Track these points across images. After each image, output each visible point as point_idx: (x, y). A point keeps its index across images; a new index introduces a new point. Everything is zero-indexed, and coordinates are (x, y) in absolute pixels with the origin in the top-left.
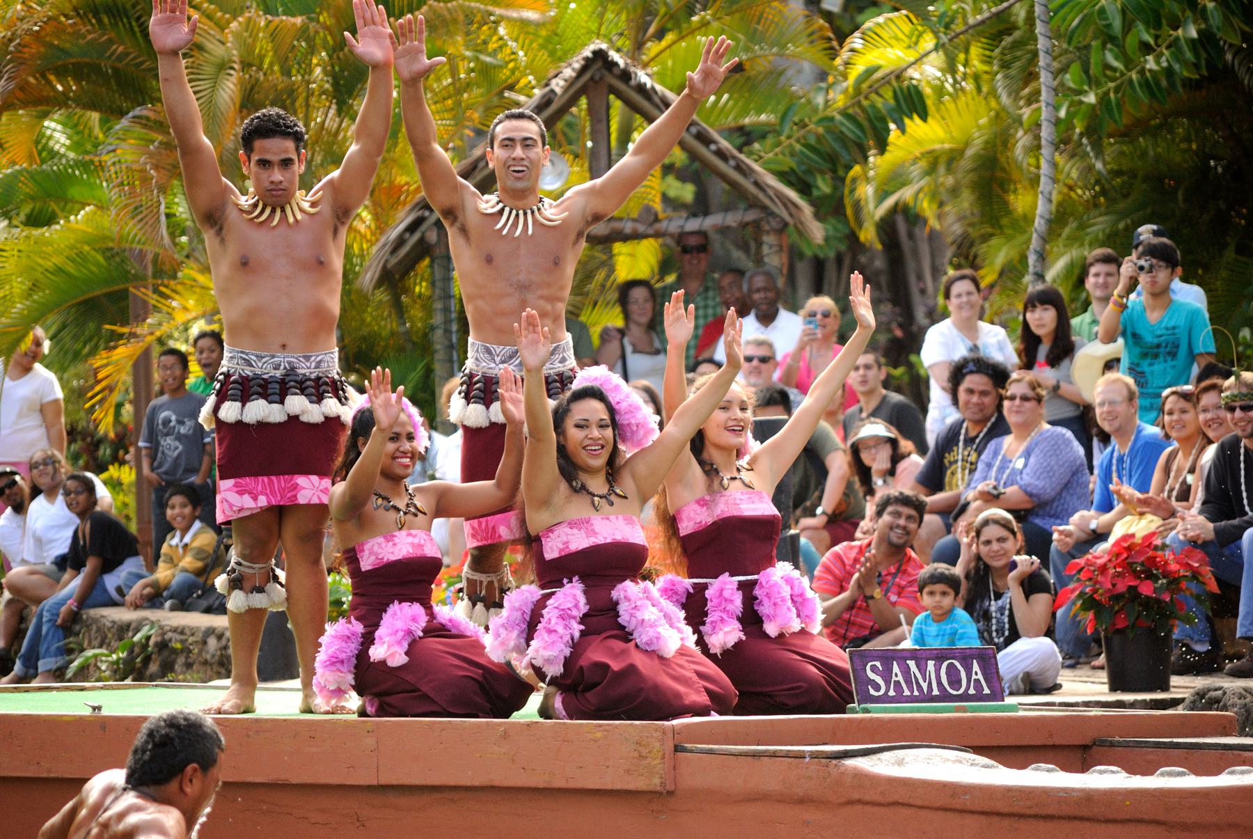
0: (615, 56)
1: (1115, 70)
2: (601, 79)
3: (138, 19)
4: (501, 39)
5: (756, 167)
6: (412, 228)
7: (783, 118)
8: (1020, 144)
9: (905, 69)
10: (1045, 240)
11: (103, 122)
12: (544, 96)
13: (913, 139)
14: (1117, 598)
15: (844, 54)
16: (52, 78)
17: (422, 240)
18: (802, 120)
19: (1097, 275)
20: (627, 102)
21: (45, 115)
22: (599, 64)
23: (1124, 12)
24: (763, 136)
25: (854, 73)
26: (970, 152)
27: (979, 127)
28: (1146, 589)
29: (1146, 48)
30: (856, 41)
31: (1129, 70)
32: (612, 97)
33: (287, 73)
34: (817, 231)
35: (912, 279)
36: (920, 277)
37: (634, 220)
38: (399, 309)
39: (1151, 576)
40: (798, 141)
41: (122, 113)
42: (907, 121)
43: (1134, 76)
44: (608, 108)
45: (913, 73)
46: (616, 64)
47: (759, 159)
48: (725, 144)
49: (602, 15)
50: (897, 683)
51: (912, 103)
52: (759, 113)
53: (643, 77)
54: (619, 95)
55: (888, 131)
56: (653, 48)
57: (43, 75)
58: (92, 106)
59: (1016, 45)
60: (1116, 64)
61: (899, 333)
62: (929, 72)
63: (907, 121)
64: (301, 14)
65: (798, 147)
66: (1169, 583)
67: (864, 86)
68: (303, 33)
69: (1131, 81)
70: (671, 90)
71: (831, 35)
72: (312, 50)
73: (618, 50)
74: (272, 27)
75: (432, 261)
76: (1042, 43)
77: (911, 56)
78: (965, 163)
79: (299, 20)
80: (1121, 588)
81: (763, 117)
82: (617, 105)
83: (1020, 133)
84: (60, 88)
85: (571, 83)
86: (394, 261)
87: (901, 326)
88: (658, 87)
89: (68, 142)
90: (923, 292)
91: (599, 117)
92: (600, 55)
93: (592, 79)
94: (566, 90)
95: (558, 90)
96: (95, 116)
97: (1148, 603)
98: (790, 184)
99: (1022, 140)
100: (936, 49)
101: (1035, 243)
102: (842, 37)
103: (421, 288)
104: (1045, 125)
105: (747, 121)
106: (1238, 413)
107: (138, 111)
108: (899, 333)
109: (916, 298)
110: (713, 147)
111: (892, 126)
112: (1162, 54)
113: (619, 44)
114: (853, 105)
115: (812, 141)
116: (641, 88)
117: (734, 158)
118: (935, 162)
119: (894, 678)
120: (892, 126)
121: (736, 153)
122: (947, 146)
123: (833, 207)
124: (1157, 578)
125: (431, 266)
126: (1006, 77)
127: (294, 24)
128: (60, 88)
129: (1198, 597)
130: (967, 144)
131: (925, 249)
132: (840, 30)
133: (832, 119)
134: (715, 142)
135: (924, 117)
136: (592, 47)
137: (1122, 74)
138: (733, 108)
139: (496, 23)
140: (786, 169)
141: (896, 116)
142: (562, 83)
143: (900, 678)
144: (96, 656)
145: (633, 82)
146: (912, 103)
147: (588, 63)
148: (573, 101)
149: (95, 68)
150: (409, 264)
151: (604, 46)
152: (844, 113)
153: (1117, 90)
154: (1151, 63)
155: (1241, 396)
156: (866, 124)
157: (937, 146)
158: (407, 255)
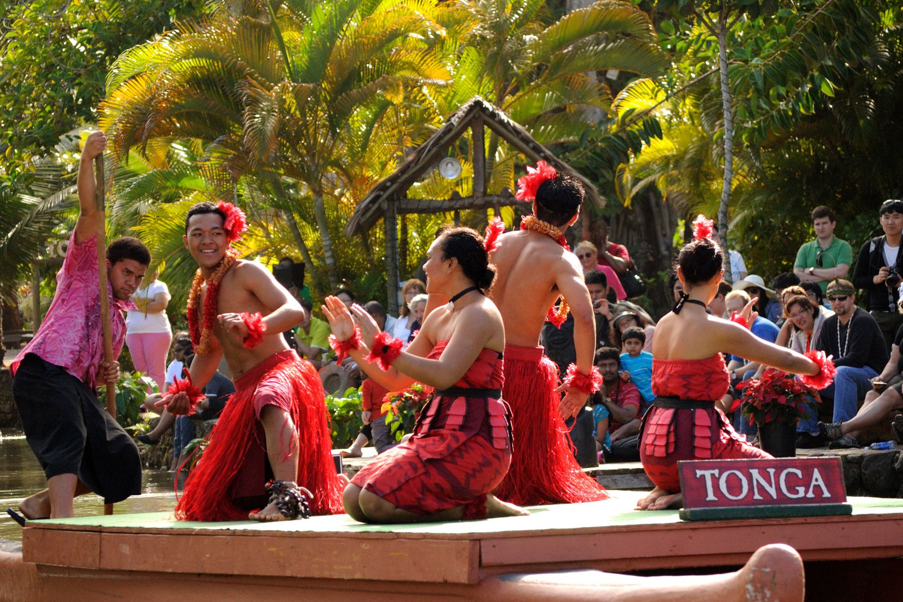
0: (486, 104)
1: (762, 109)
2: (479, 117)
3: (222, 87)
4: (424, 95)
5: (566, 165)
6: (373, 201)
7: (581, 139)
8: (714, 152)
9: (650, 110)
10: (727, 205)
11: (203, 144)
12: (447, 127)
13: (657, 148)
14: (767, 405)
15: (616, 102)
16: (174, 120)
17: (379, 208)
18: (592, 139)
19: (818, 224)
20: (494, 130)
21: (172, 141)
22: (478, 108)
23: (765, 77)
24: (574, 149)
25: (621, 113)
26: (688, 156)
27: (693, 143)
28: (782, 400)
29: (780, 98)
30: (623, 94)
31: (772, 110)
32: (486, 127)
33: (304, 115)
34: (602, 201)
35: (659, 228)
36: (663, 228)
37: (498, 196)
38: (367, 247)
39: (784, 393)
40: (590, 151)
41: (213, 140)
42: (651, 139)
43: (774, 113)
44: (483, 133)
45: (653, 113)
46: (488, 109)
47: (568, 161)
48: (548, 152)
49: (481, 81)
50: (817, 487)
51: (653, 129)
52: (569, 136)
53: (503, 116)
54: (490, 126)
55: (641, 145)
56: (509, 99)
57: (169, 118)
58: (197, 136)
59: (710, 99)
60: (764, 106)
61: (651, 259)
62: (662, 114)
63: (651, 139)
64: (312, 82)
65: (589, 154)
66: (795, 397)
67: (627, 120)
68: (313, 93)
69: (772, 116)
70: (519, 123)
71: (609, 92)
72: (317, 102)
73: (490, 101)
74: (297, 89)
75: (385, 220)
76: (725, 96)
77: (652, 103)
78: (685, 164)
79: (311, 86)
80: (768, 400)
81: (571, 138)
82: (488, 131)
83: (714, 147)
84: (178, 125)
85: (462, 119)
86: (363, 220)
87: (652, 255)
88: (512, 122)
89: (186, 156)
90: (664, 236)
91: (479, 138)
92: (478, 104)
93: (474, 117)
94: (459, 123)
95: (455, 124)
96: (199, 142)
97: (782, 408)
98: (586, 175)
99: (715, 151)
100: (667, 99)
101: (722, 207)
102: (615, 93)
103: (379, 234)
104: (727, 142)
105: (562, 140)
106: (837, 301)
107: (221, 138)
108: (651, 259)
109: (661, 240)
110: (542, 155)
111: (643, 142)
112: (789, 101)
113: (490, 97)
114: (620, 131)
115: (598, 150)
116: (501, 122)
117: (554, 161)
118: (666, 161)
119: (814, 483)
120: (643, 142)
121: (556, 158)
122: (675, 152)
123: (608, 189)
124: (788, 394)
125: (385, 223)
126: (706, 115)
127: (309, 88)
128: (178, 125)
129: (811, 405)
130: (686, 152)
131: (665, 211)
132: (616, 87)
133: (610, 138)
134: (544, 152)
135: (661, 138)
136: (473, 100)
137: (768, 112)
138: (555, 132)
139: (421, 87)
140: (583, 166)
141: (645, 136)
142: (457, 120)
143: (821, 483)
144: (199, 442)
145: (497, 119)
146: (653, 129)
147: (472, 108)
148: (464, 129)
149: (198, 114)
150: (372, 223)
151: (480, 99)
152: (616, 135)
153: (765, 121)
154: (782, 105)
155: (839, 292)
156: (628, 141)
157: (667, 153)
158: (371, 216)
